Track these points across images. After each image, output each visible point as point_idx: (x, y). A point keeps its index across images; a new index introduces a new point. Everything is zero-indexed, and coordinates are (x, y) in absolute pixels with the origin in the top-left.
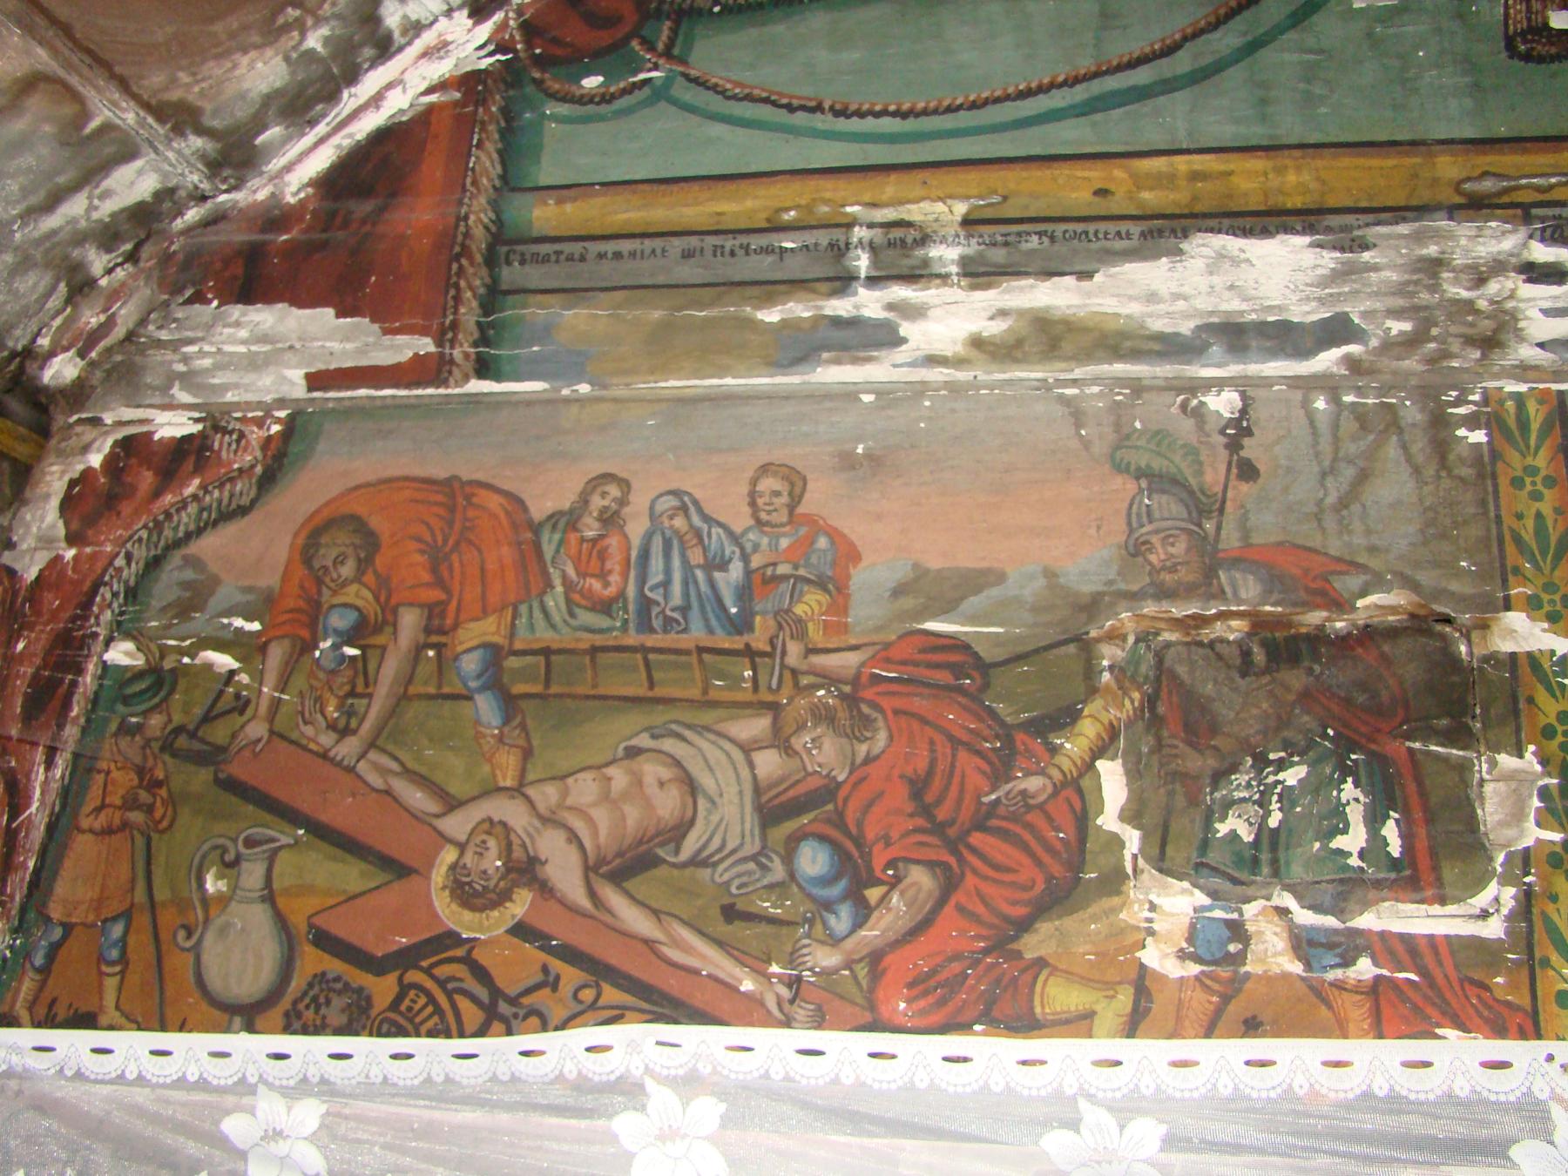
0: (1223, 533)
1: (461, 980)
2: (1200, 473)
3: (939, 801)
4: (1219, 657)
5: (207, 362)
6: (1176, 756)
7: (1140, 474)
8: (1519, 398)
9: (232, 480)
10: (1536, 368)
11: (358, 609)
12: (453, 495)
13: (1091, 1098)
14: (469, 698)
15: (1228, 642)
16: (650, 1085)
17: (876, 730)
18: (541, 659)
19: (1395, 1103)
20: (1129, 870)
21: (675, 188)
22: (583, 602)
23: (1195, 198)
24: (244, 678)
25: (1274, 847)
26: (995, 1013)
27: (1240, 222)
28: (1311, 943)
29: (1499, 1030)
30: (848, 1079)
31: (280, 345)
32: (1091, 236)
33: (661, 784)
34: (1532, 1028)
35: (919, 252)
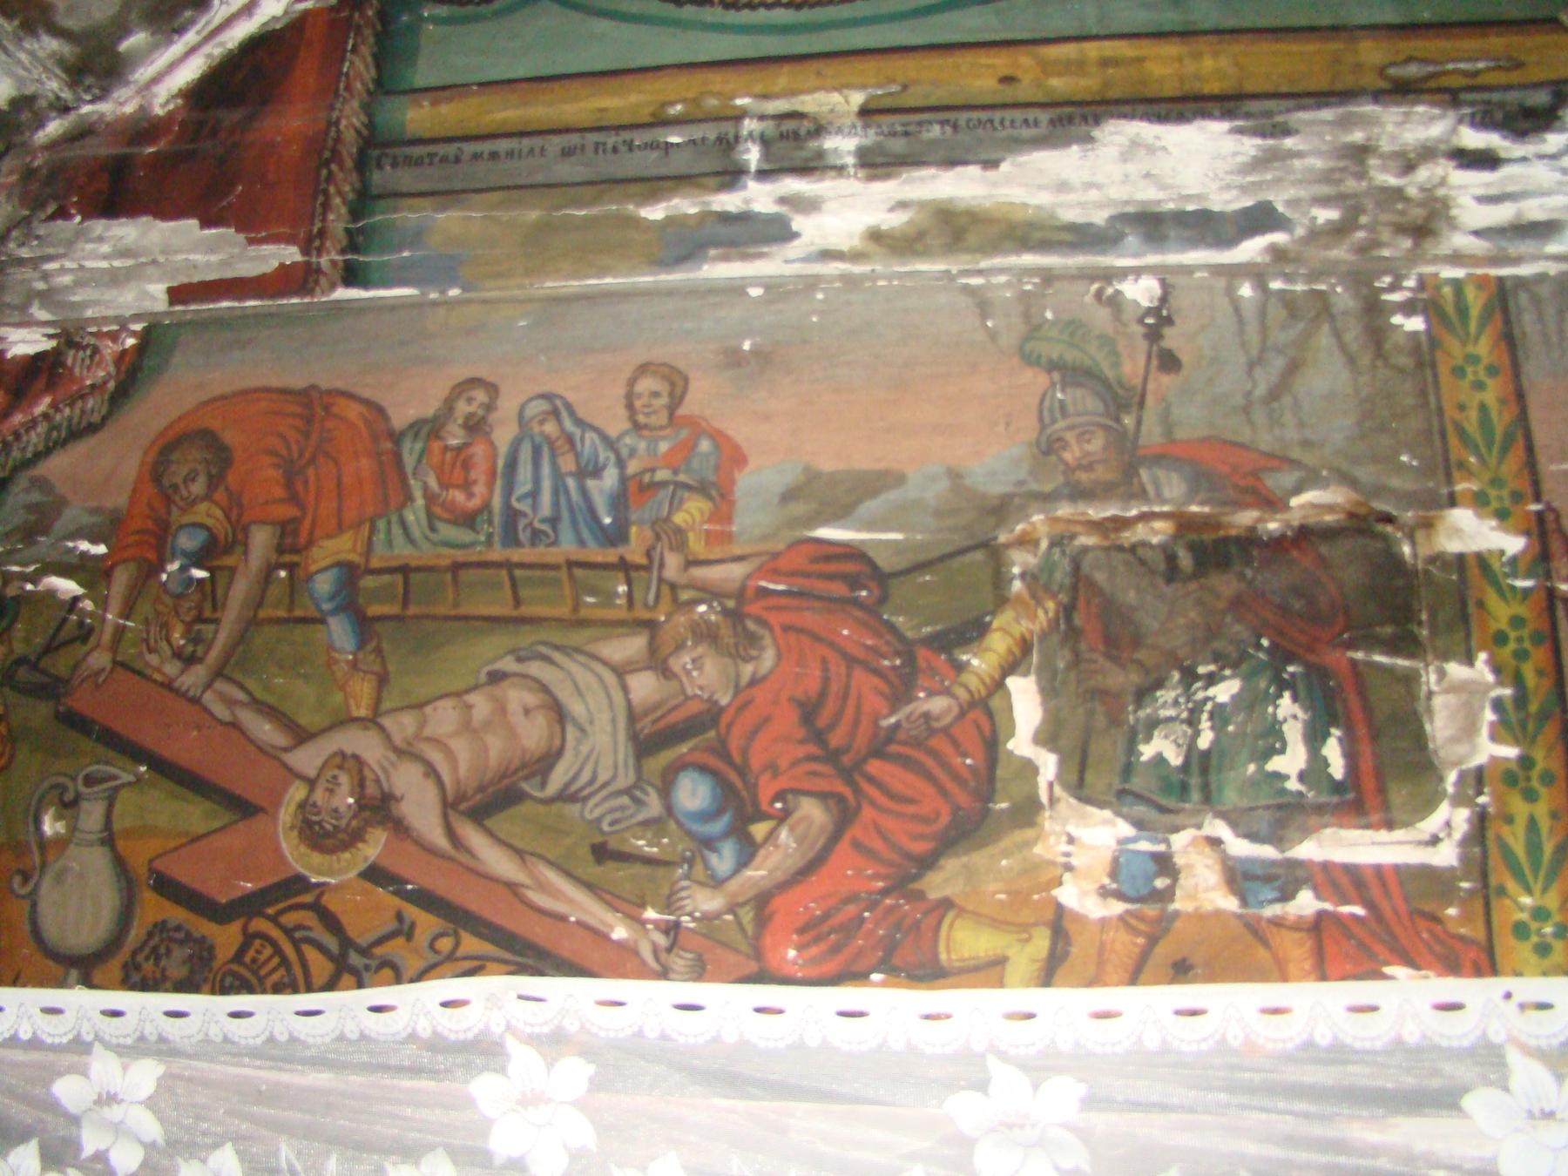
0: (1144, 428)
1: (309, 928)
2: (1117, 364)
3: (832, 726)
4: (1142, 562)
5: (67, 279)
6: (1096, 672)
7: (1052, 366)
8: (1457, 284)
9: (83, 397)
10: (1472, 257)
11: (208, 529)
12: (312, 405)
13: (1002, 1056)
14: (323, 621)
15: (1151, 546)
16: (511, 1044)
17: (762, 649)
18: (399, 578)
19: (1338, 1054)
20: (1044, 798)
21: (556, 85)
22: (445, 515)
23: (1107, 84)
24: (88, 605)
25: (1205, 770)
26: (896, 961)
27: (1156, 108)
28: (1249, 876)
29: (1451, 965)
30: (730, 1037)
31: (143, 260)
32: (997, 124)
33: (527, 712)
34: (1487, 963)
35: (813, 144)
